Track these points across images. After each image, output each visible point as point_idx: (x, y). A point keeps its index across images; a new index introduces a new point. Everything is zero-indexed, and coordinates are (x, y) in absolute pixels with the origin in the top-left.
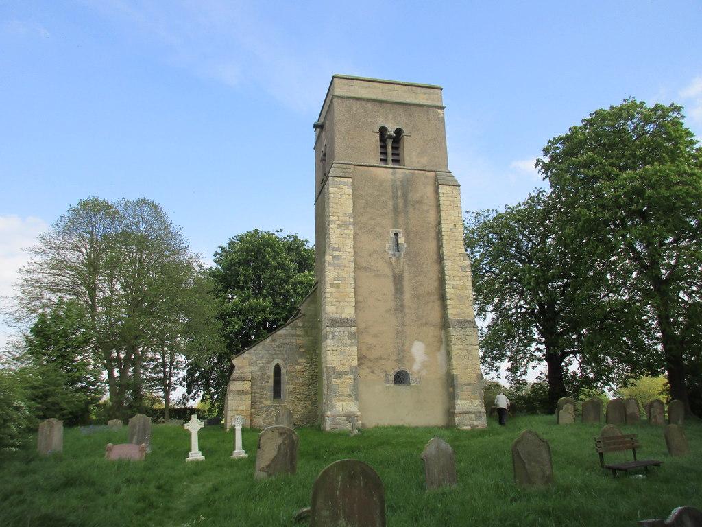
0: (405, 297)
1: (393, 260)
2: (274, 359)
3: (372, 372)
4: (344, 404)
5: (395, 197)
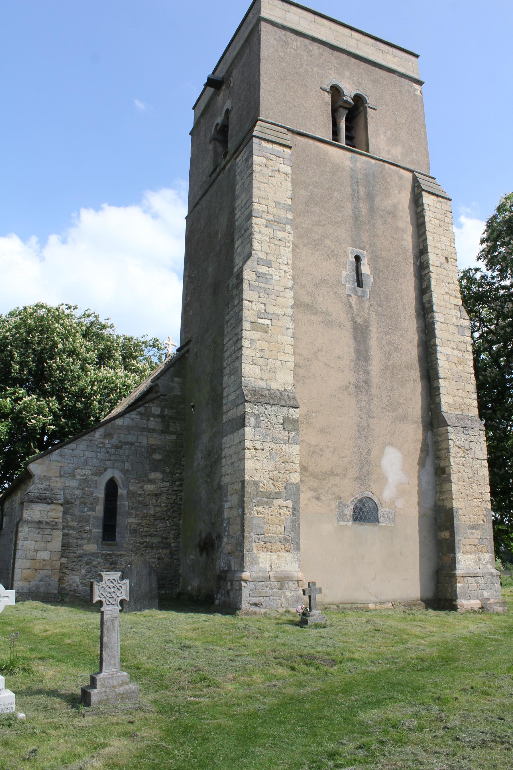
0: (372, 368)
1: (354, 300)
2: (106, 469)
3: (317, 499)
4: (274, 556)
5: (355, 197)
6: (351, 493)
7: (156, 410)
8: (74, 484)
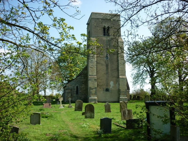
2: (76, 85)
3: (100, 88)
6: (105, 87)
7: (83, 76)
8: (72, 87)
